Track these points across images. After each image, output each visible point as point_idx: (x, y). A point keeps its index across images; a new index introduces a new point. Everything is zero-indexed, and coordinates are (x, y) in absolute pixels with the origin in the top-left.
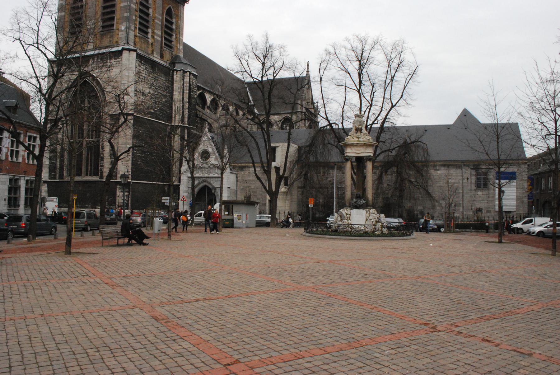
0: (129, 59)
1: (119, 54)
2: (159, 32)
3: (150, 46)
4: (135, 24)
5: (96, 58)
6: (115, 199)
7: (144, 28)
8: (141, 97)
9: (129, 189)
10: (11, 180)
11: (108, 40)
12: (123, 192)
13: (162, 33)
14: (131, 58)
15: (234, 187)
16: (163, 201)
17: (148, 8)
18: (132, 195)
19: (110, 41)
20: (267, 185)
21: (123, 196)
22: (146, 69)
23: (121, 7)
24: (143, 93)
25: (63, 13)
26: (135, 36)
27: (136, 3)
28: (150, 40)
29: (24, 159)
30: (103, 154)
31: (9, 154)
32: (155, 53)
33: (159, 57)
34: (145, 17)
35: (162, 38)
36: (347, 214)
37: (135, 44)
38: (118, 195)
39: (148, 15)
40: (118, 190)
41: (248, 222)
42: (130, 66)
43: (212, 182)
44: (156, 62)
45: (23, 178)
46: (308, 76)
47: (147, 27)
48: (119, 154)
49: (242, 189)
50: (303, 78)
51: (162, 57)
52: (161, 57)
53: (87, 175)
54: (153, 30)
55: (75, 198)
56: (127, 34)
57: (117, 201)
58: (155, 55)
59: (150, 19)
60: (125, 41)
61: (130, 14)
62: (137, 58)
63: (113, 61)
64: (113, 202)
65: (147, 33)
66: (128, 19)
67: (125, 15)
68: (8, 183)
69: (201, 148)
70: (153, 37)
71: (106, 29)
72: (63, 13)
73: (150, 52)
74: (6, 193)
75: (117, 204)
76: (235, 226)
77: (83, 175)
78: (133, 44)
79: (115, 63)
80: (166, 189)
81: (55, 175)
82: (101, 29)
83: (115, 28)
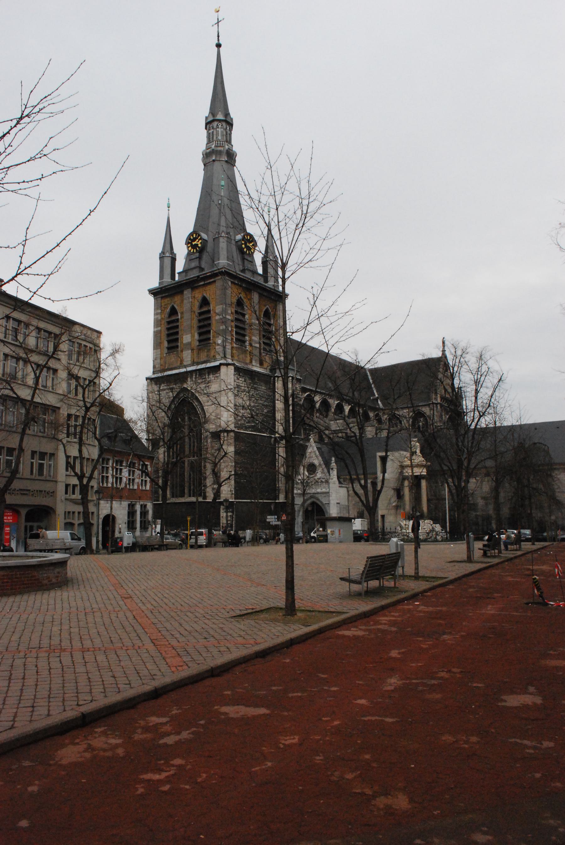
0: (227, 374)
1: (217, 369)
2: (256, 338)
3: (248, 356)
4: (232, 335)
5: (194, 374)
6: (219, 519)
7: (240, 339)
8: (242, 411)
9: (233, 509)
10: (129, 505)
11: (205, 354)
12: (227, 512)
13: (260, 339)
14: (229, 372)
15: (344, 502)
16: (268, 520)
17: (244, 315)
18: (236, 515)
19: (208, 355)
20: (363, 499)
21: (227, 516)
22: (245, 381)
23: (216, 320)
24: (243, 407)
25: (159, 328)
26: (232, 348)
27: (232, 313)
28: (248, 348)
29: (138, 486)
30: (205, 473)
31: (127, 482)
32: (254, 361)
33: (258, 365)
34: (241, 325)
35: (260, 344)
36: (405, 525)
37: (232, 356)
38: (221, 516)
39: (244, 322)
40: (222, 511)
41: (342, 535)
42: (229, 381)
43: (320, 498)
44: (255, 371)
45: (138, 503)
46: (444, 356)
47: (244, 336)
48: (222, 480)
49: (354, 505)
50: (438, 360)
51: (261, 364)
52: (260, 365)
53: (190, 496)
54: (250, 337)
55: (189, 519)
56: (224, 347)
57: (221, 522)
58: (254, 363)
59: (247, 327)
60: (222, 355)
61: (226, 327)
62: (235, 371)
63: (211, 376)
64: (218, 524)
65: (244, 342)
66: (224, 333)
67: (221, 328)
68: (127, 509)
69: (306, 461)
70: (251, 345)
71: (202, 343)
72: (159, 328)
73: (248, 361)
74: (126, 518)
75: (221, 524)
76: (329, 540)
77: (186, 496)
78: (230, 357)
79: (213, 378)
80: (272, 507)
81: (158, 497)
82: (198, 343)
83: (211, 342)
